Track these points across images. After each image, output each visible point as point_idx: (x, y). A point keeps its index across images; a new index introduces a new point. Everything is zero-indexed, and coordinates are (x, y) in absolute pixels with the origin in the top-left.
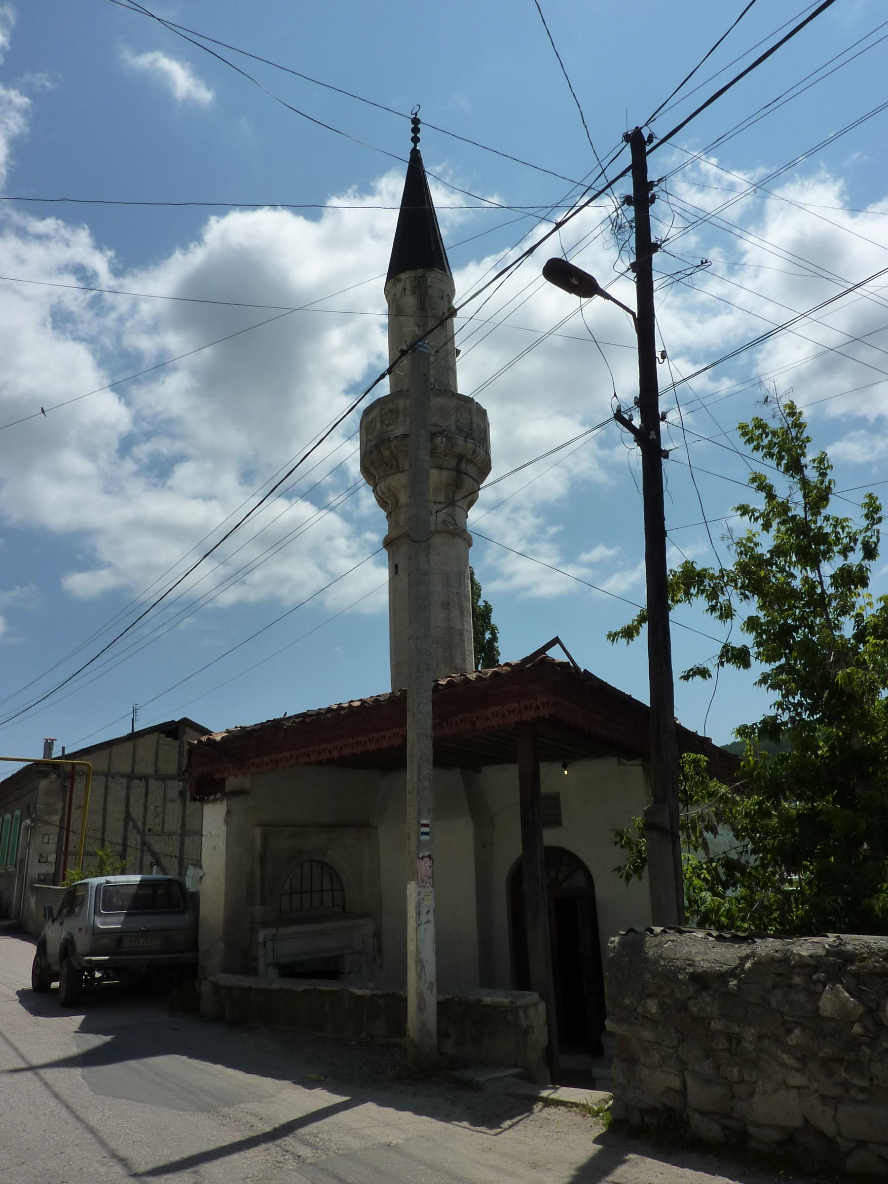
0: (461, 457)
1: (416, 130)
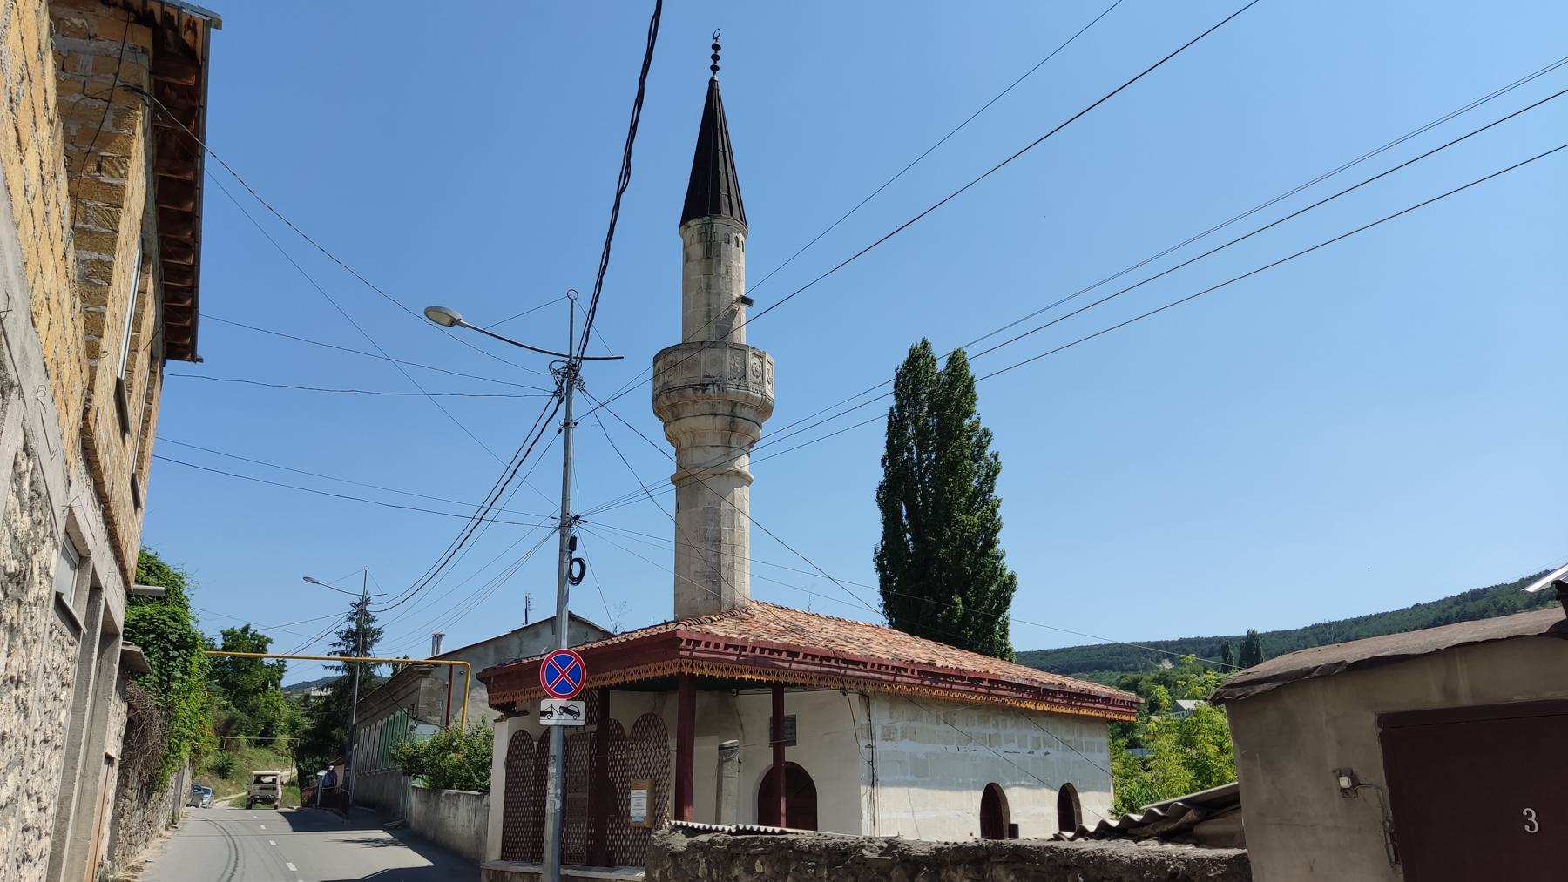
0: (734, 404)
1: (715, 58)
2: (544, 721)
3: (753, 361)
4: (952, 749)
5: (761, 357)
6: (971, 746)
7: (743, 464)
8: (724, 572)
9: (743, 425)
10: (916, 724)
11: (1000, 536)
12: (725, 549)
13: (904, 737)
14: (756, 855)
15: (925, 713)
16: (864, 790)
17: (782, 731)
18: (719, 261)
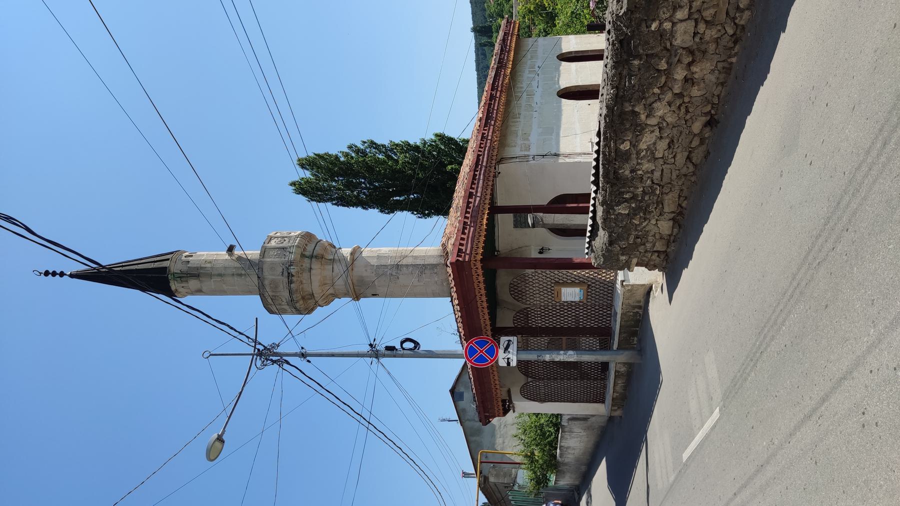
0: (303, 256)
1: (54, 274)
2: (514, 363)
3: (273, 243)
4: (535, 114)
5: (271, 239)
6: (534, 105)
7: (346, 251)
8: (419, 262)
9: (318, 250)
10: (520, 133)
11: (412, 143)
12: (404, 262)
13: (528, 139)
14: (617, 150)
15: (513, 129)
16: (561, 160)
17: (520, 212)
18: (201, 268)
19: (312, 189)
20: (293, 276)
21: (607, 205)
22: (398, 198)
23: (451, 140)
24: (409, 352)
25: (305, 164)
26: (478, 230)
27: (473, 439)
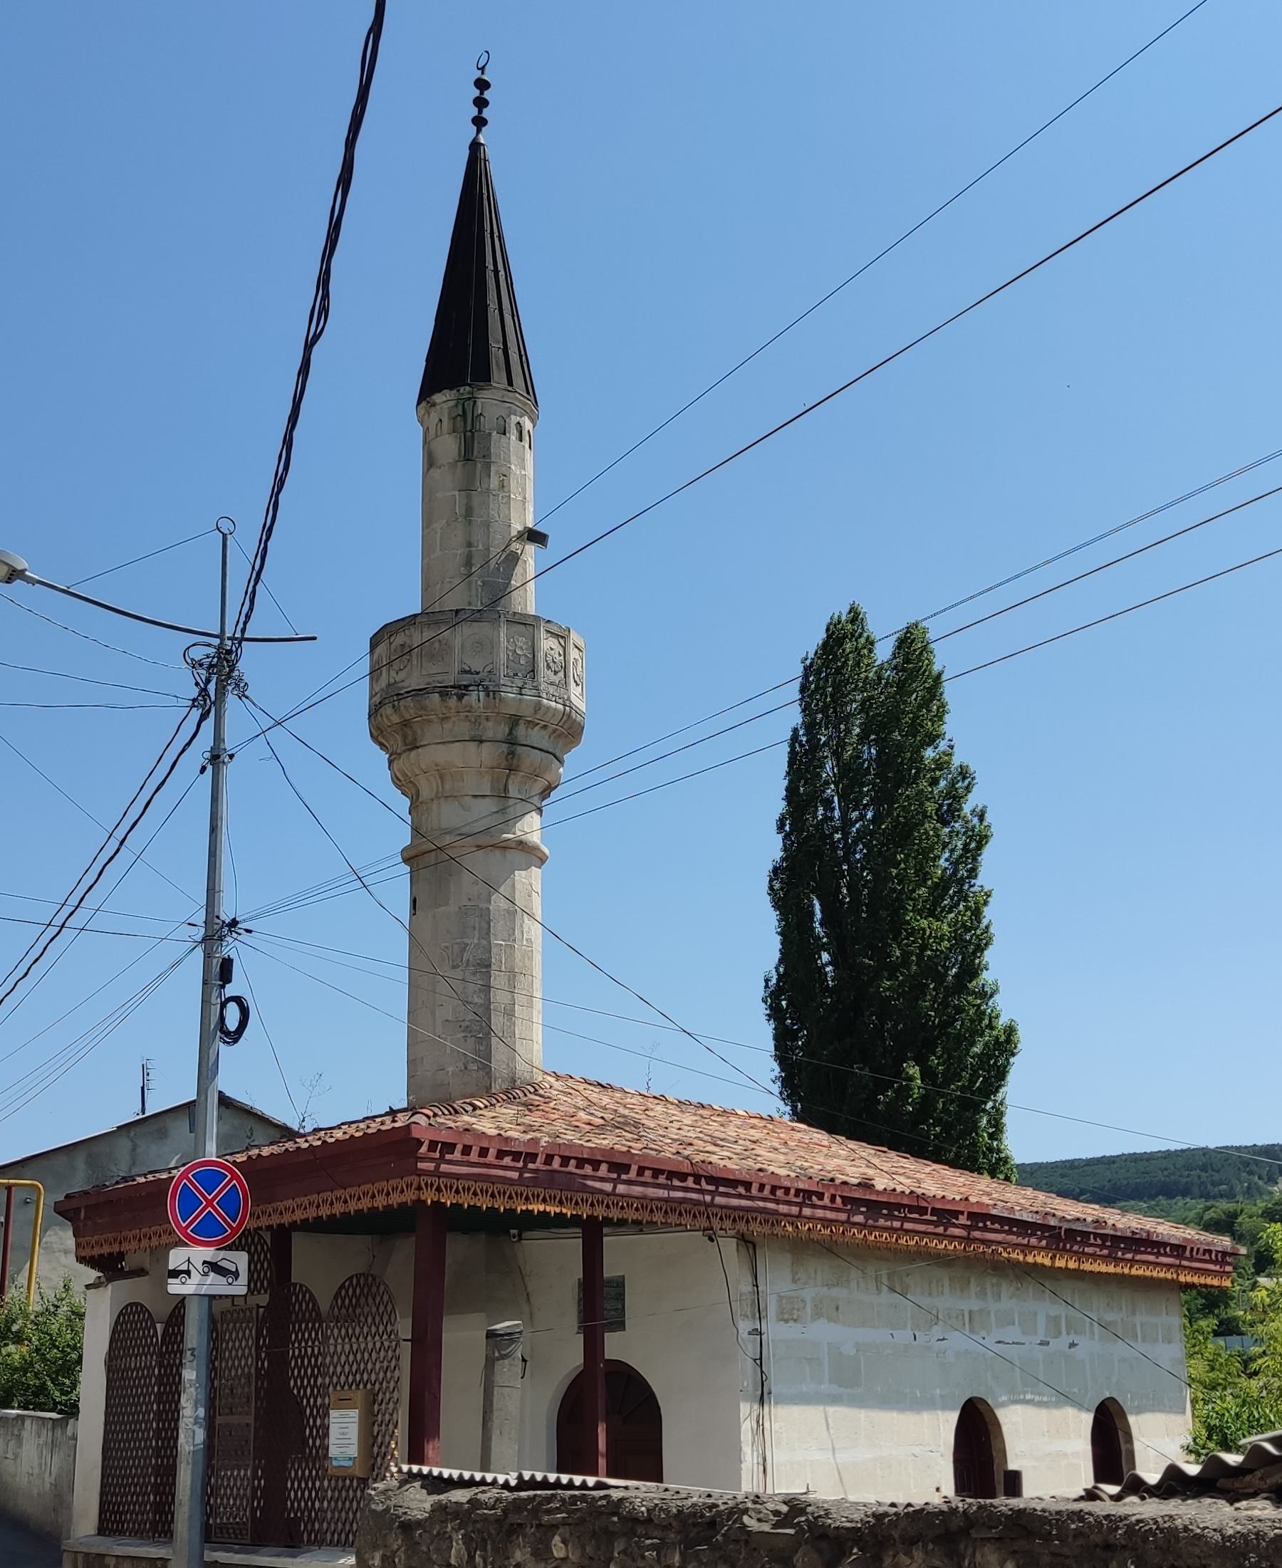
0: (514, 721)
1: (481, 103)
3: (547, 644)
4: (904, 1336)
6: (937, 1331)
7: (531, 827)
8: (497, 1021)
9: (530, 758)
11: (989, 956)
12: (498, 980)
13: (817, 1315)
14: (554, 1527)
15: (854, 1274)
16: (746, 1410)
18: (487, 466)
19: (839, 671)
20: (460, 697)
21: (469, 1512)
22: (818, 915)
23: (1000, 1075)
24: (214, 1019)
25: (911, 646)
26: (511, 1190)
27: (80, 1162)
